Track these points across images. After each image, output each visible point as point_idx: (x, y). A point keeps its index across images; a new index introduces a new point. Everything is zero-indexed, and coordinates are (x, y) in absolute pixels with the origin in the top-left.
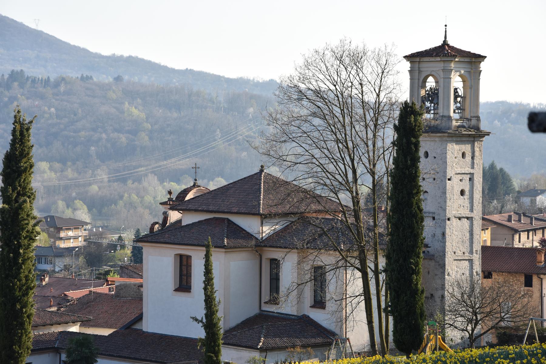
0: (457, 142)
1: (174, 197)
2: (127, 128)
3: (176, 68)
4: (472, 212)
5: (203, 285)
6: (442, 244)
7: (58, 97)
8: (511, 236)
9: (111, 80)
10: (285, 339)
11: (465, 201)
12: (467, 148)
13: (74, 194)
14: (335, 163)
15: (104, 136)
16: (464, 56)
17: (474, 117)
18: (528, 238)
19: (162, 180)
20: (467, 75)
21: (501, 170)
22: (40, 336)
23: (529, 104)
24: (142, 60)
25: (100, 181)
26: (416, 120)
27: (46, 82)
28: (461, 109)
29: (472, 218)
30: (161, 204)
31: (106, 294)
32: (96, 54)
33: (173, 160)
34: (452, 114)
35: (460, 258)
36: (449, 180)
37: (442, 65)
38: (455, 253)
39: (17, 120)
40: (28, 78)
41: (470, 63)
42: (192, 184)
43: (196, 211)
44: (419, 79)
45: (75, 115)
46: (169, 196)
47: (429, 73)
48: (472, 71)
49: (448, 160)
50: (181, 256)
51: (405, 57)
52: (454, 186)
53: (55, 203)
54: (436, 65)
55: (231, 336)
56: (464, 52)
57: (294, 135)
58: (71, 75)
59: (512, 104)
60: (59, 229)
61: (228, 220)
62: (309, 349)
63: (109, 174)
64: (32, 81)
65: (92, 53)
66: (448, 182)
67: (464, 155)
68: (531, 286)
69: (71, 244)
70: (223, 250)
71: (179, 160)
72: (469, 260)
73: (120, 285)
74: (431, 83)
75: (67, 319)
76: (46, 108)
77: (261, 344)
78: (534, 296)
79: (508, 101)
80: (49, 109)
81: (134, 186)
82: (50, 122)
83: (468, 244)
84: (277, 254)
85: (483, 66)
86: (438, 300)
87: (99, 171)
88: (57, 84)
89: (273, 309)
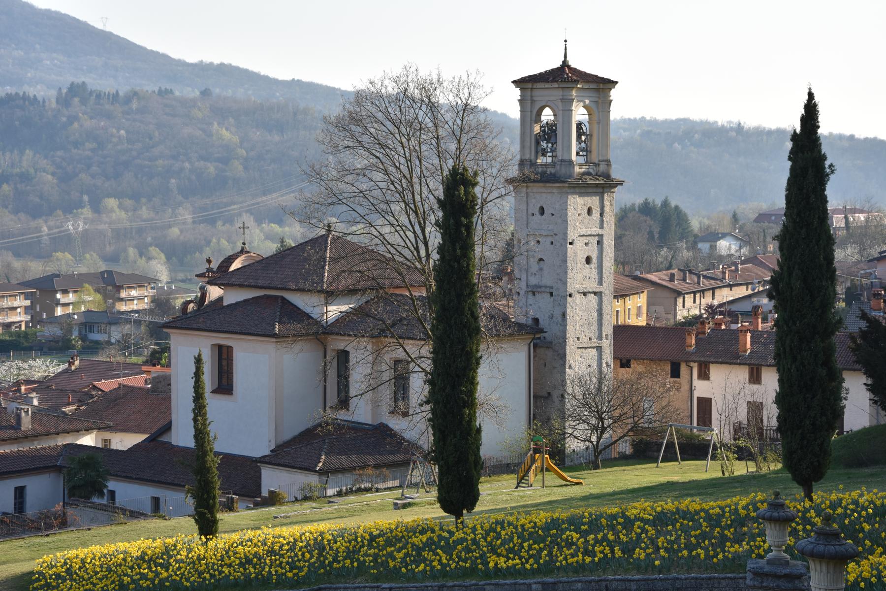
0: (581, 194)
1: (215, 265)
2: (216, 155)
3: (280, 78)
4: (601, 284)
5: (192, 415)
6: (561, 328)
7: (129, 117)
8: (673, 300)
9: (198, 93)
10: (354, 457)
12: (593, 201)
13: (149, 239)
14: (401, 233)
15: (187, 165)
16: (588, 82)
17: (603, 161)
18: (694, 302)
19: (259, 221)
20: (593, 106)
21: (677, 207)
22: (37, 450)
23: (716, 122)
24: (237, 68)
25: (181, 223)
26: (467, 193)
27: (115, 98)
28: (585, 151)
29: (601, 292)
30: (197, 276)
31: (140, 388)
32: (179, 61)
33: (274, 195)
34: (574, 157)
35: (585, 346)
36: (571, 244)
37: (559, 93)
38: (578, 339)
40: (91, 93)
41: (597, 90)
42: (239, 249)
43: (241, 286)
44: (531, 111)
45: (151, 139)
46: (207, 266)
47: (543, 104)
48: (600, 101)
49: (569, 218)
50: (220, 347)
51: (514, 82)
52: (577, 252)
53: (125, 250)
54: (553, 92)
55: (283, 454)
56: (590, 75)
57: (346, 195)
58: (146, 88)
59: (696, 122)
60: (119, 288)
61: (283, 298)
62: (384, 470)
63: (194, 213)
64: (97, 96)
65: (174, 60)
66: (569, 246)
67: (590, 211)
68: (678, 376)
69: (135, 306)
70: (274, 340)
71: (282, 196)
72: (597, 348)
73: (158, 377)
74: (547, 115)
75: (79, 425)
76: (114, 130)
77: (320, 464)
78: (682, 389)
79: (691, 118)
80: (118, 132)
81: (224, 228)
82: (119, 147)
83: (596, 326)
84: (340, 343)
85: (614, 93)
86: (556, 400)
87: (181, 210)
88: (128, 99)
89: (343, 415)
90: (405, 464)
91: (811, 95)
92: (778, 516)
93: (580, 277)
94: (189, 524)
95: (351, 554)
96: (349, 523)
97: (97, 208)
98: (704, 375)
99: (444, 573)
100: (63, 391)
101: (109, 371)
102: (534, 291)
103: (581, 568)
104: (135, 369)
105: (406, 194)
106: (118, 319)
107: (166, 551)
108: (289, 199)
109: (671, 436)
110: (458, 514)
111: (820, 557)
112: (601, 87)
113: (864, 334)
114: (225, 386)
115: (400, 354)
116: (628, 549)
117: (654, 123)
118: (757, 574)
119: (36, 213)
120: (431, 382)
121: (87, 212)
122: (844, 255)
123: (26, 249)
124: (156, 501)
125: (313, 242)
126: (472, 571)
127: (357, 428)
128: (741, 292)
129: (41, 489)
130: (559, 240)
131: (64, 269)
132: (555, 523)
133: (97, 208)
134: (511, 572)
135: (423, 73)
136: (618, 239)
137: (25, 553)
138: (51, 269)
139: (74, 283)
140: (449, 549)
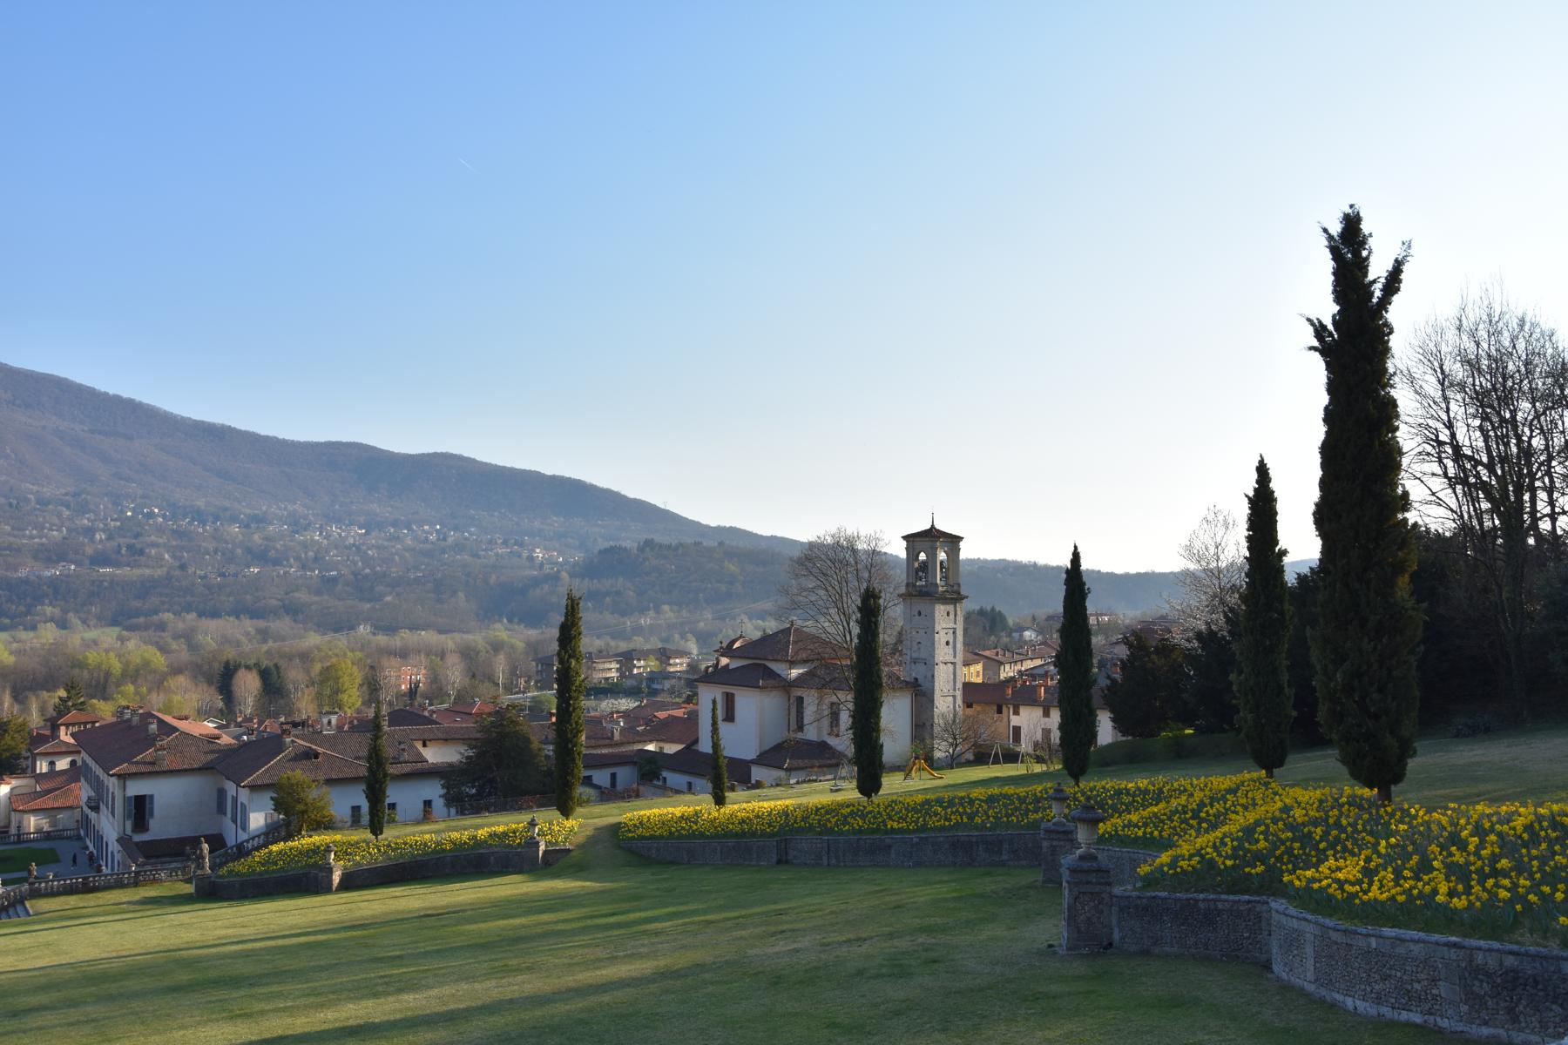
11: (949, 650)
12: (950, 608)
19: (751, 619)
27: (670, 546)
28: (945, 577)
39: (570, 598)
69: (678, 668)
74: (922, 556)
85: (962, 544)
88: (677, 548)
89: (800, 735)
90: (837, 765)
91: (1263, 471)
92: (1060, 797)
93: (942, 653)
94: (709, 798)
95: (804, 819)
96: (804, 800)
97: (657, 610)
98: (1016, 713)
99: (860, 831)
100: (637, 718)
101: (663, 706)
102: (915, 661)
103: (943, 828)
104: (678, 706)
105: (838, 603)
106: (668, 676)
107: (696, 814)
108: (768, 605)
109: (997, 749)
110: (869, 796)
111: (1083, 821)
112: (953, 541)
113: (1109, 688)
114: (730, 717)
115: (834, 699)
116: (971, 817)
117: (986, 561)
118: (1048, 831)
119: (623, 614)
120: (853, 717)
121: (652, 613)
122: (1097, 640)
123: (619, 635)
124: (690, 784)
125: (782, 631)
126: (878, 830)
127: (809, 743)
128: (1038, 662)
129: (625, 774)
130: (930, 631)
131: (638, 646)
132: (927, 802)
133: (657, 610)
134: (901, 831)
135: (849, 532)
136: (965, 630)
137: (616, 811)
138: (631, 646)
139: (644, 655)
140: (863, 817)
